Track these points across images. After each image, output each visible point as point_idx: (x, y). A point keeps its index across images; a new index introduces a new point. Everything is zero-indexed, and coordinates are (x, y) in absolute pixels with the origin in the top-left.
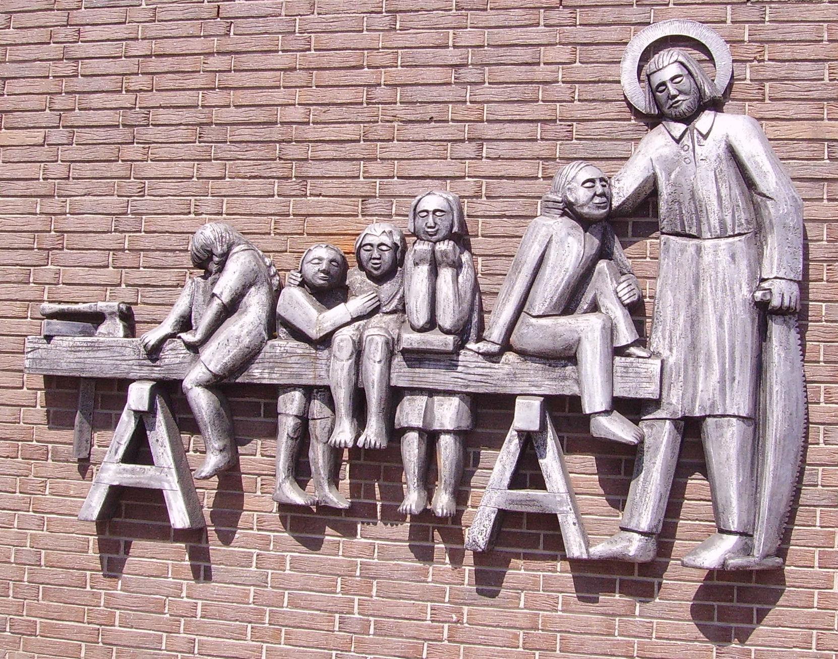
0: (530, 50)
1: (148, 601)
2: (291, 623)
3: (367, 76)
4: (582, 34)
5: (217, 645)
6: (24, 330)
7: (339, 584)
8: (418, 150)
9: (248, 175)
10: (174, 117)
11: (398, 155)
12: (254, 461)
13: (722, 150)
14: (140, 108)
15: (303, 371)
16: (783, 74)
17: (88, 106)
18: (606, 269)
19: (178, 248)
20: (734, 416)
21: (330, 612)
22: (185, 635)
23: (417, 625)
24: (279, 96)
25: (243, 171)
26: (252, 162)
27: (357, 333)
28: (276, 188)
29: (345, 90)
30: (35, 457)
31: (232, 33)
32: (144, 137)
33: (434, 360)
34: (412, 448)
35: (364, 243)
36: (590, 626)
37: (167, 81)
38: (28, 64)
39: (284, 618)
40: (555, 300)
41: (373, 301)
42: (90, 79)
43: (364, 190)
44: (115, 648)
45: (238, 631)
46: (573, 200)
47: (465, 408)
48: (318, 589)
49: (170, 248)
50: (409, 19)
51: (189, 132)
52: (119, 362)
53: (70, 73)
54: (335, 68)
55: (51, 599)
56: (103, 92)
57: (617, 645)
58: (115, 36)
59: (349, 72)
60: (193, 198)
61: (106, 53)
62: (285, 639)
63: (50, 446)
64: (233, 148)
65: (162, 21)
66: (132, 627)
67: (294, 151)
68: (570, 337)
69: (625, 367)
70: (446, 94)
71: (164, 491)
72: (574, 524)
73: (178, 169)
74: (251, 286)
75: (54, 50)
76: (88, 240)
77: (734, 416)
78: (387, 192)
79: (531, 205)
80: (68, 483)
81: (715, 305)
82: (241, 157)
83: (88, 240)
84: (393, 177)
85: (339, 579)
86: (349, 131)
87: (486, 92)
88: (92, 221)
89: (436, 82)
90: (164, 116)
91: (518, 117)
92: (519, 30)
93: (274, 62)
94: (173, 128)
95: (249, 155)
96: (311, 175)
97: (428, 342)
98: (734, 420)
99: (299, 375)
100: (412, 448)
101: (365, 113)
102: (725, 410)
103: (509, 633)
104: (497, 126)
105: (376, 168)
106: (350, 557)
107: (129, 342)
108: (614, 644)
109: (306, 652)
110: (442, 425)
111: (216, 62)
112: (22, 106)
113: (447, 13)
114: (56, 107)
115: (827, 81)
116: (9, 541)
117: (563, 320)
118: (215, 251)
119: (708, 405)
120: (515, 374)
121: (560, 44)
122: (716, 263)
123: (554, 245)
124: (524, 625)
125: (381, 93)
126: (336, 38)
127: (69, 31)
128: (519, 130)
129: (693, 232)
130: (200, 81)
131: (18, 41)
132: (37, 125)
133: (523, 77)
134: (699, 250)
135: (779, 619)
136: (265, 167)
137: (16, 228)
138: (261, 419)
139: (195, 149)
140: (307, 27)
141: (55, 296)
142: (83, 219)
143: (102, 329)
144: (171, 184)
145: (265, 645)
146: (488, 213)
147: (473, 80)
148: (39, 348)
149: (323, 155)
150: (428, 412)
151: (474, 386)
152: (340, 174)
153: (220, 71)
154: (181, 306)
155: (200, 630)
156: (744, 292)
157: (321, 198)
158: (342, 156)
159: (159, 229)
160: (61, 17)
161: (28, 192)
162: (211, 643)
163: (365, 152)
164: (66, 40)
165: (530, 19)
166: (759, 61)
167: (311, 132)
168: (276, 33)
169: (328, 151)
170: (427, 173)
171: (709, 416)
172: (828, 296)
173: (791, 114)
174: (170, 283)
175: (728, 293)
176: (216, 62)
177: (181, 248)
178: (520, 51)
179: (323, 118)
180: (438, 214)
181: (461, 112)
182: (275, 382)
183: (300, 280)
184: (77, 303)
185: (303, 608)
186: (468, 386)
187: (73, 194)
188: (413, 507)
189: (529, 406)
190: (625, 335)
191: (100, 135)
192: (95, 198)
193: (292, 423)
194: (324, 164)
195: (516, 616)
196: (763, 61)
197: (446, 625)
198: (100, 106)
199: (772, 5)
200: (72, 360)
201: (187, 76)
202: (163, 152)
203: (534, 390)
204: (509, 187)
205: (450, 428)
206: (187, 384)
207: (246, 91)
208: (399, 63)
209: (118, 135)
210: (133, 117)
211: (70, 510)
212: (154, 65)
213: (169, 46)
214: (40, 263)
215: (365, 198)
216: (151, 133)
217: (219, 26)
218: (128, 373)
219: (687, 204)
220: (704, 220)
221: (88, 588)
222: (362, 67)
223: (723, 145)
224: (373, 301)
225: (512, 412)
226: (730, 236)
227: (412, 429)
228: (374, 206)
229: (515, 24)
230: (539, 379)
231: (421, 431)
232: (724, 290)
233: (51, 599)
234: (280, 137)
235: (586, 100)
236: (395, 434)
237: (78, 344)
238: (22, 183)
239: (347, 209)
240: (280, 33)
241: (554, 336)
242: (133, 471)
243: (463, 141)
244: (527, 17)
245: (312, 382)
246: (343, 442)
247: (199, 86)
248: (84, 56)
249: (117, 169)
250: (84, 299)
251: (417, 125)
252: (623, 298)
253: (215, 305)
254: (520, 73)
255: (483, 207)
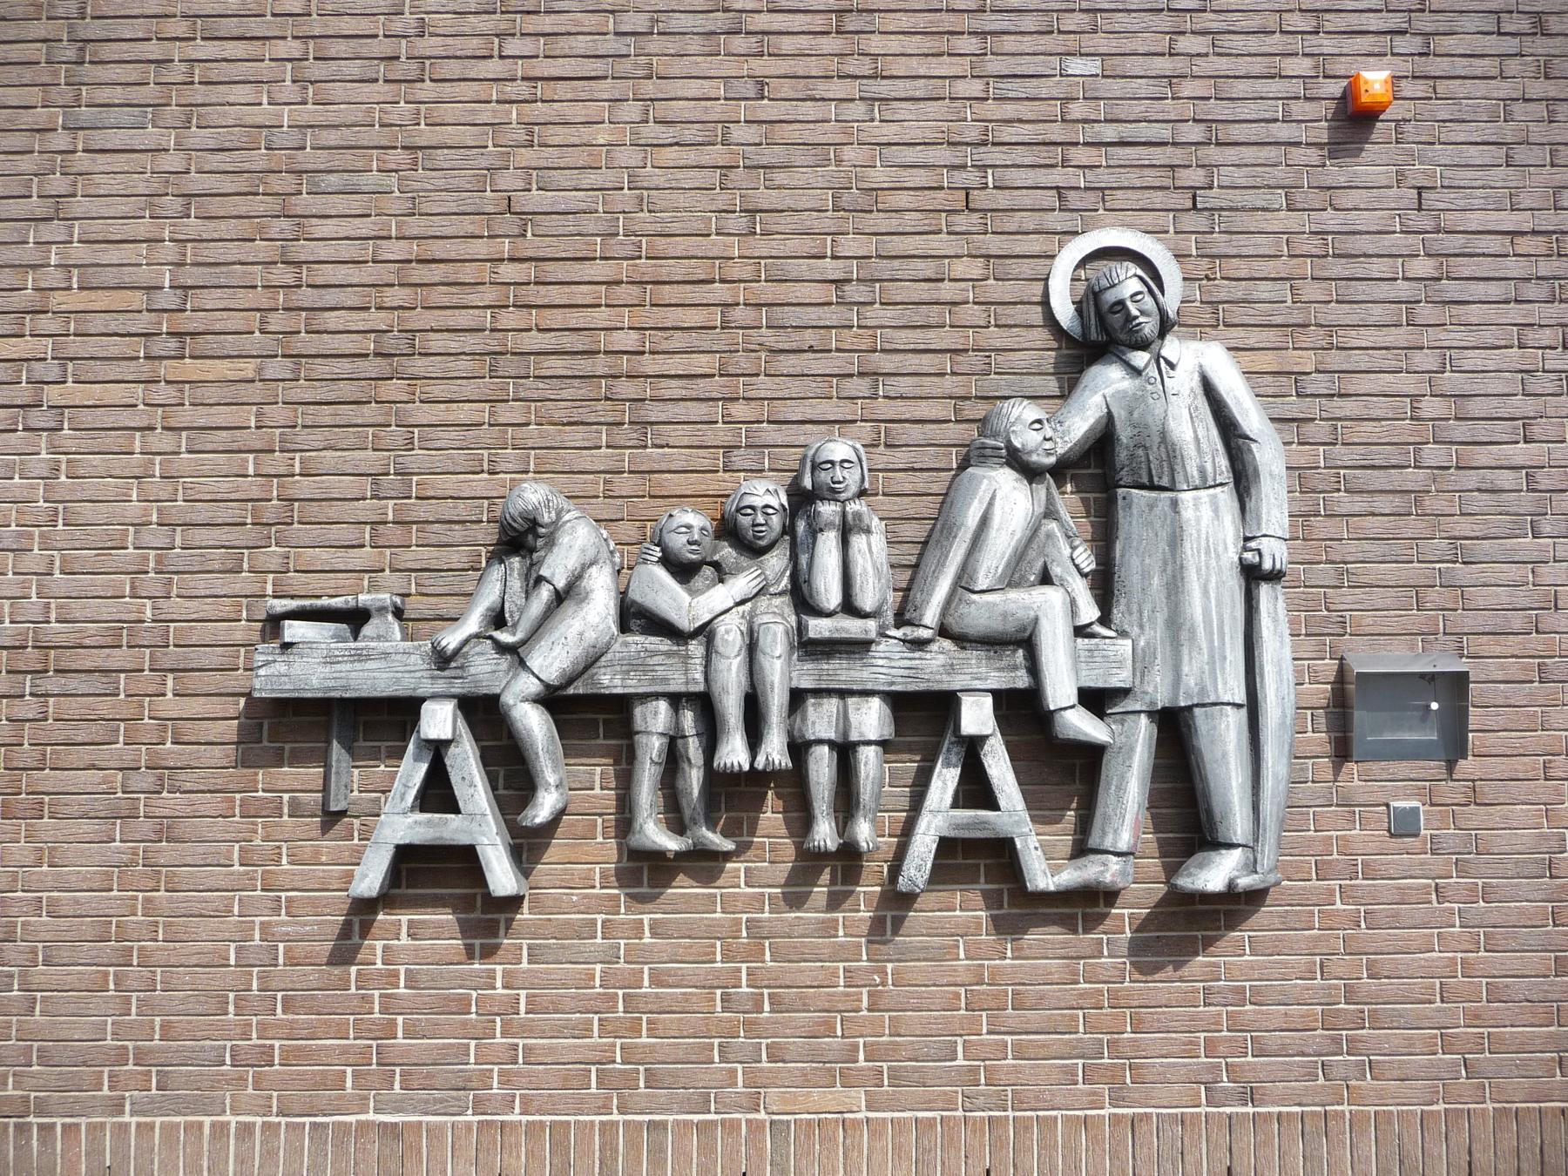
0: (931, 263)
1: (447, 998)
2: (654, 1007)
3: (720, 292)
4: (994, 244)
5: (551, 1048)
6: (239, 637)
7: (719, 949)
8: (795, 387)
9: (565, 420)
10: (453, 344)
11: (769, 394)
12: (594, 796)
13: (1196, 382)
14: (399, 331)
15: (669, 675)
16: (1240, 295)
17: (322, 328)
18: (1056, 530)
19: (468, 518)
20: (1228, 704)
21: (710, 988)
22: (504, 1040)
23: (828, 994)
24: (601, 317)
25: (558, 415)
26: (569, 403)
27: (743, 621)
28: (604, 437)
29: (693, 310)
30: (263, 813)
31: (529, 234)
32: (410, 371)
33: (847, 653)
34: (822, 766)
35: (742, 505)
36: (1050, 973)
37: (439, 296)
38: (224, 269)
39: (646, 1003)
40: (1000, 570)
41: (759, 579)
42: (323, 291)
43: (726, 438)
44: (398, 1069)
45: (581, 1027)
46: (1019, 446)
47: (887, 711)
48: (691, 959)
49: (456, 518)
50: (774, 220)
51: (477, 364)
52: (400, 675)
53: (291, 282)
54: (678, 282)
55: (297, 1011)
56: (343, 308)
57: (1083, 995)
58: (358, 233)
59: (697, 288)
60: (485, 453)
61: (346, 256)
62: (648, 1030)
63: (286, 797)
64: (541, 385)
65: (427, 214)
66: (424, 1037)
67: (626, 388)
68: (1025, 615)
69: (1089, 651)
70: (830, 316)
71: (478, 848)
72: (1036, 848)
73: (464, 413)
74: (592, 564)
75: (261, 250)
76: (334, 511)
77: (1228, 704)
78: (757, 441)
79: (944, 455)
80: (318, 846)
81: (1199, 570)
82: (553, 397)
83: (334, 511)
84: (762, 422)
85: (718, 943)
86: (702, 363)
87: (876, 315)
88: (337, 485)
89: (813, 301)
90: (437, 342)
91: (922, 347)
92: (917, 237)
93: (592, 272)
94: (452, 358)
95: (565, 394)
96: (653, 419)
97: (843, 629)
98: (1229, 708)
99: (665, 680)
100: (822, 766)
101: (719, 340)
102: (1218, 697)
103: (948, 992)
104: (897, 357)
105: (740, 410)
106: (734, 913)
107: (415, 648)
108: (1081, 994)
109: (679, 1044)
110: (861, 734)
111: (509, 272)
112: (218, 327)
113: (822, 214)
114: (271, 328)
115: (1289, 303)
116: (227, 935)
117: (1013, 595)
118: (540, 520)
119: (1196, 690)
120: (952, 665)
121: (968, 256)
122: (1198, 520)
123: (998, 503)
124: (967, 981)
125: (740, 315)
126: (677, 243)
127: (285, 224)
128: (924, 362)
129: (1165, 482)
130: (489, 295)
131: (205, 236)
132: (244, 353)
133: (926, 297)
134: (1175, 504)
135: (1277, 946)
136: (588, 410)
137: (219, 497)
138: (601, 741)
139: (484, 387)
140: (637, 228)
141: (285, 588)
142: (323, 482)
143: (368, 630)
144: (453, 434)
145: (619, 1041)
146: (891, 466)
147: (862, 300)
148: (275, 661)
149: (667, 394)
150: (844, 720)
151: (900, 684)
152: (693, 419)
153: (515, 284)
154: (489, 597)
155: (527, 1030)
156: (1232, 555)
157: (666, 450)
158: (694, 394)
159: (439, 493)
160: (273, 204)
161: (235, 446)
162: (543, 1047)
163: (725, 390)
164: (282, 236)
165: (930, 225)
166: (1209, 279)
167: (649, 365)
168: (592, 235)
169: (674, 389)
170: (809, 417)
171: (1197, 705)
172: (1307, 557)
173: (1251, 342)
174: (460, 566)
175: (1213, 555)
176: (509, 272)
177: (474, 518)
178: (919, 264)
179: (665, 346)
180: (846, 465)
181: (849, 339)
182: (632, 690)
183: (660, 555)
184: (319, 597)
185: (671, 986)
186: (893, 683)
187: (306, 447)
188: (829, 843)
189: (980, 706)
190: (1089, 612)
191: (343, 367)
192: (339, 453)
193: (657, 744)
194: (670, 405)
195: (955, 971)
196: (1215, 279)
197: (865, 990)
198: (341, 328)
199: (1223, 213)
200: (327, 675)
201: (468, 289)
202: (438, 390)
203: (978, 684)
204: (916, 433)
205: (873, 737)
206: (508, 699)
207: (555, 311)
208: (763, 278)
209: (372, 367)
210: (391, 343)
211: (323, 883)
212: (419, 273)
213: (438, 249)
214: (260, 544)
215: (729, 448)
216: (419, 365)
217: (509, 224)
218: (414, 689)
219: (1155, 449)
220: (1178, 468)
221: (353, 990)
222: (712, 281)
223: (1196, 377)
224: (759, 579)
225: (1000, 713)
226: (1211, 487)
227: (820, 742)
228: (740, 459)
229: (913, 230)
230: (983, 670)
231: (832, 744)
232: (1208, 552)
233: (297, 1011)
234: (607, 371)
235: (1005, 326)
236: (799, 748)
237: (337, 653)
238: (224, 433)
239: (706, 464)
240: (597, 235)
241: (1005, 615)
242: (429, 822)
243: (851, 375)
244: (926, 222)
245: (683, 689)
246: (736, 764)
247: (487, 303)
248: (311, 259)
249: (370, 413)
250: (332, 592)
251: (792, 356)
252: (1082, 566)
253: (545, 593)
254: (922, 291)
255: (885, 459)
